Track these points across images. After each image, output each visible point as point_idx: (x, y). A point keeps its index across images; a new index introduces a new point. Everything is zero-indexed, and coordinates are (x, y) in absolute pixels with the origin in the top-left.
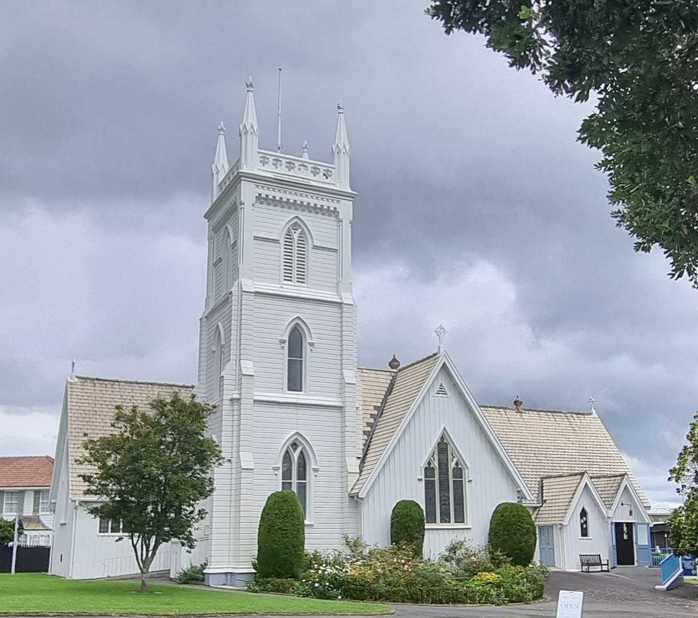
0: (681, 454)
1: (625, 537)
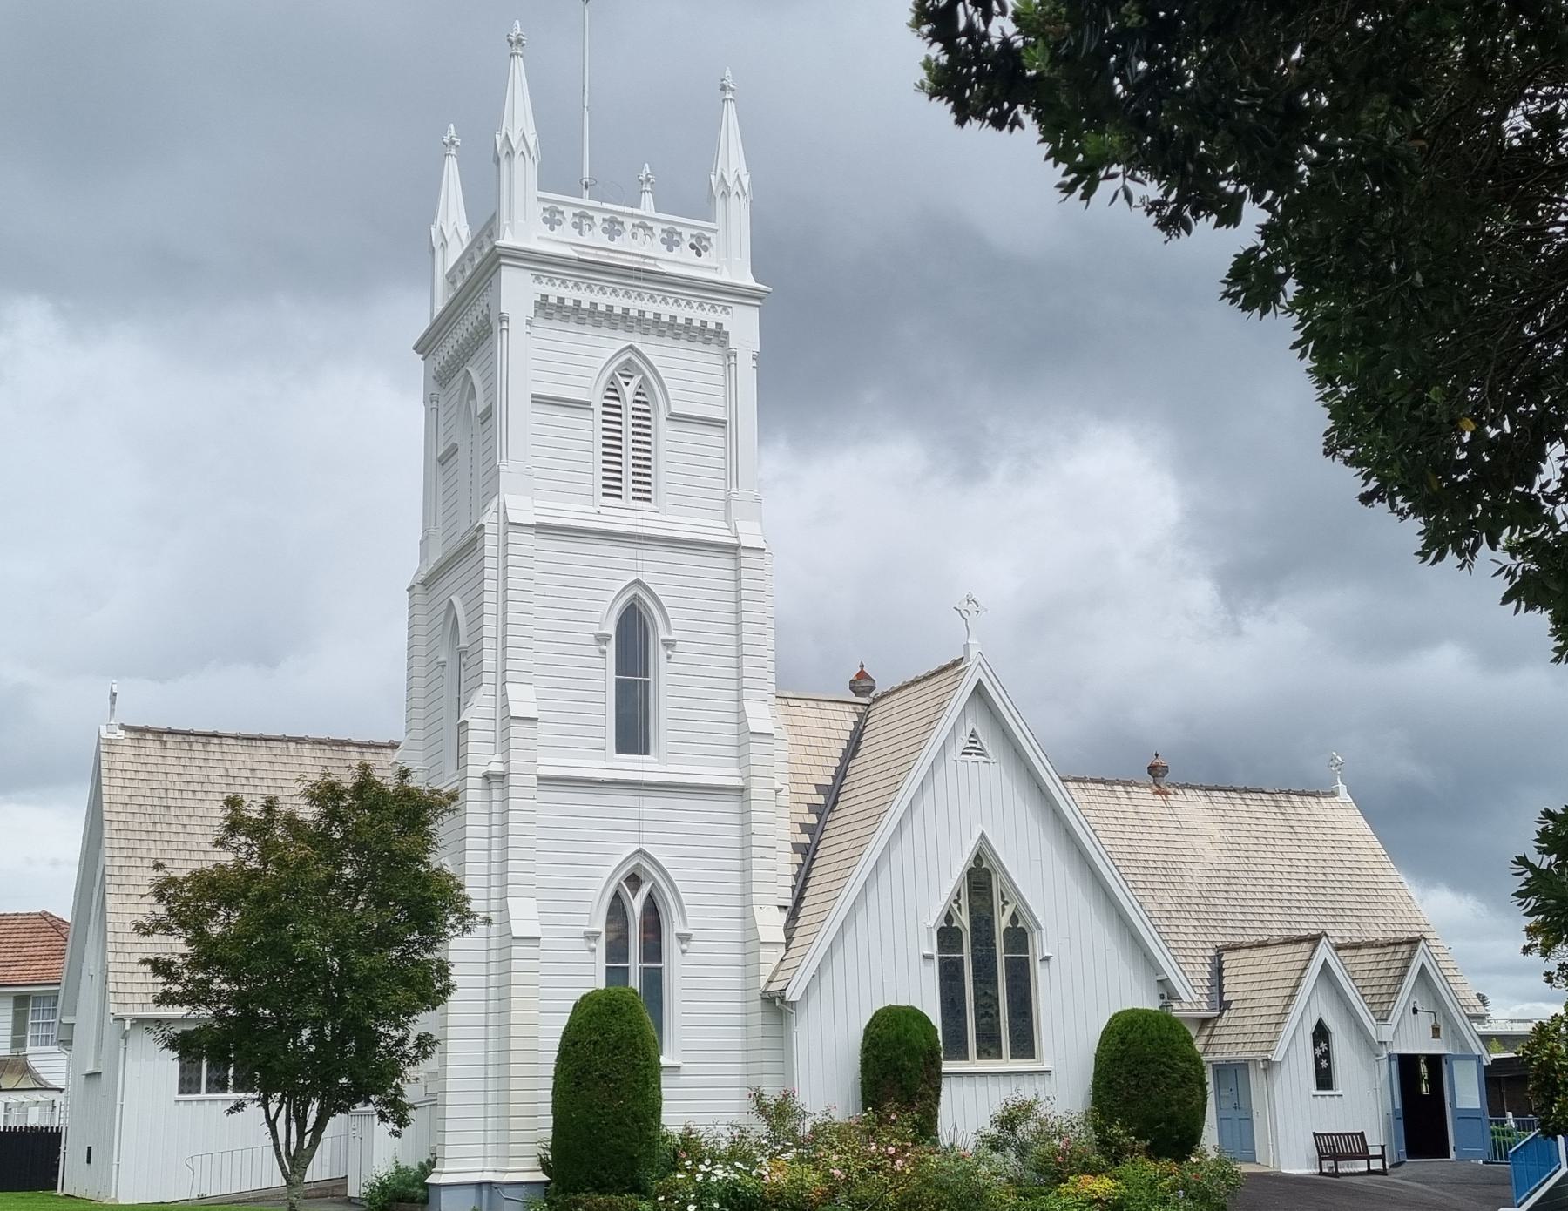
1: (1425, 1089)
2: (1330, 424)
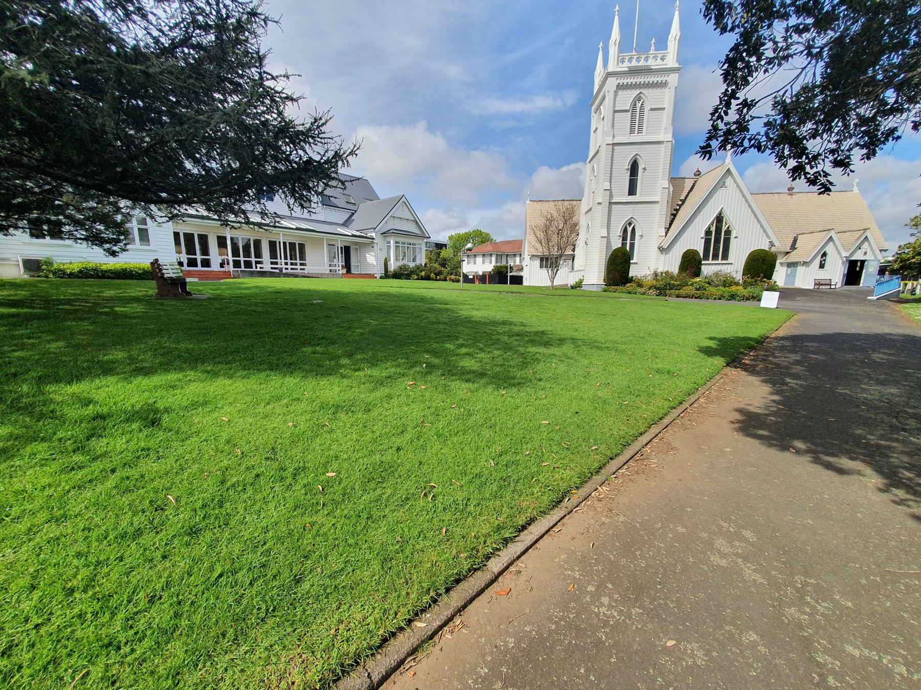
1: (858, 269)
2: (481, 274)
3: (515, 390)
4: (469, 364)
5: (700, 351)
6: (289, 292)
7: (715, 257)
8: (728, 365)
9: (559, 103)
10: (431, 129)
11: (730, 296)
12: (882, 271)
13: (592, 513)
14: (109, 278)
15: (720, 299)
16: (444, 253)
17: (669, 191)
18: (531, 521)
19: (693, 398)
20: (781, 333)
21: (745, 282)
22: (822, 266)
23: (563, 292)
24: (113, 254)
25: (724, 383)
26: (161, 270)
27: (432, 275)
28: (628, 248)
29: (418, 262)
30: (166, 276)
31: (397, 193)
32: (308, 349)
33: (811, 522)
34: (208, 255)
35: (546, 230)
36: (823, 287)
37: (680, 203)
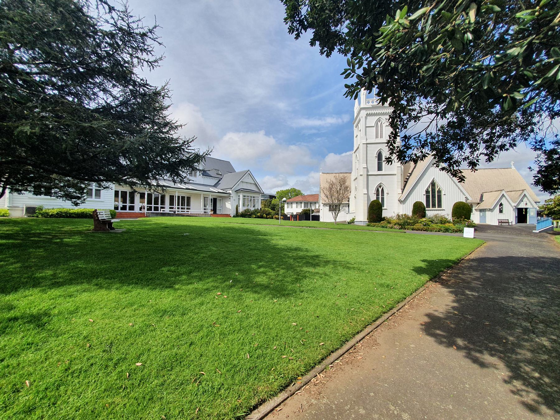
0: (422, 160)
1: (524, 213)
3: (283, 299)
4: (261, 280)
5: (413, 270)
6: (173, 227)
7: (434, 206)
8: (431, 280)
9: (340, 121)
10: (267, 134)
11: (445, 230)
12: (539, 214)
13: (306, 395)
14: (73, 217)
15: (439, 231)
16: (274, 201)
17: (401, 169)
18: (262, 402)
19: (401, 305)
20: (472, 256)
21: (454, 221)
22: (501, 211)
23: (341, 227)
24: (76, 204)
25: (425, 294)
26: (97, 216)
27: (265, 215)
28: (380, 201)
29: (256, 208)
30: (100, 218)
31: (246, 169)
32: (165, 269)
33: (451, 408)
34: (133, 203)
35: (331, 189)
36: (505, 224)
37: (409, 175)
